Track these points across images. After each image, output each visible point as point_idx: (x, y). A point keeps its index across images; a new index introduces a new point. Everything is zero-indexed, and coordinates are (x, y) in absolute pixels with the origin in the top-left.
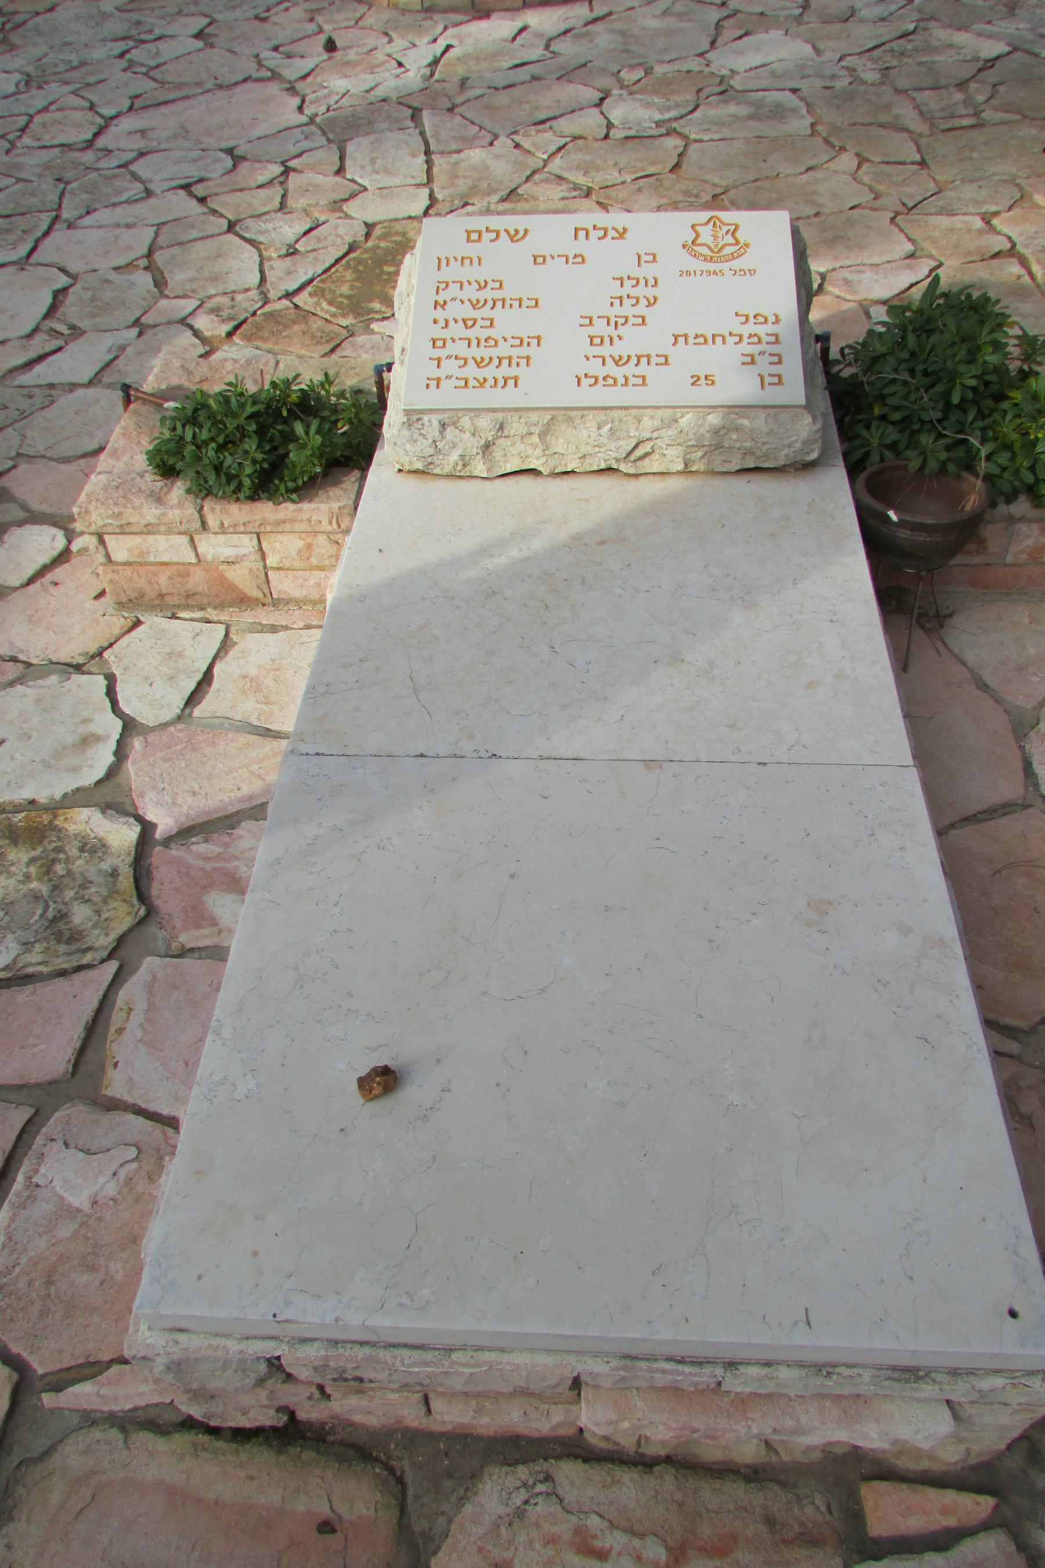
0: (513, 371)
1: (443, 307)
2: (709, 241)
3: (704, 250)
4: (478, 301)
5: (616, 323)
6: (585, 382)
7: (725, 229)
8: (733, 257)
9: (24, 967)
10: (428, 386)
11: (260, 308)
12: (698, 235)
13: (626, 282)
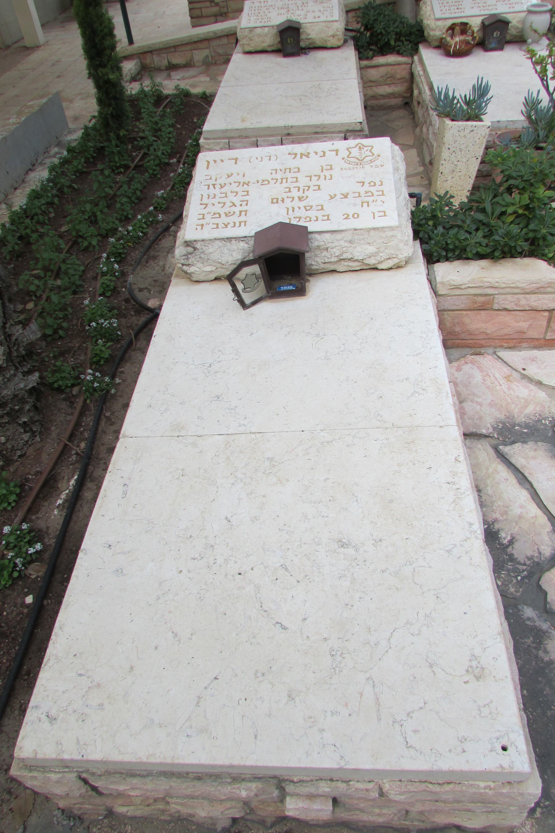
4: (230, 213)
5: (304, 189)
12: (350, 153)
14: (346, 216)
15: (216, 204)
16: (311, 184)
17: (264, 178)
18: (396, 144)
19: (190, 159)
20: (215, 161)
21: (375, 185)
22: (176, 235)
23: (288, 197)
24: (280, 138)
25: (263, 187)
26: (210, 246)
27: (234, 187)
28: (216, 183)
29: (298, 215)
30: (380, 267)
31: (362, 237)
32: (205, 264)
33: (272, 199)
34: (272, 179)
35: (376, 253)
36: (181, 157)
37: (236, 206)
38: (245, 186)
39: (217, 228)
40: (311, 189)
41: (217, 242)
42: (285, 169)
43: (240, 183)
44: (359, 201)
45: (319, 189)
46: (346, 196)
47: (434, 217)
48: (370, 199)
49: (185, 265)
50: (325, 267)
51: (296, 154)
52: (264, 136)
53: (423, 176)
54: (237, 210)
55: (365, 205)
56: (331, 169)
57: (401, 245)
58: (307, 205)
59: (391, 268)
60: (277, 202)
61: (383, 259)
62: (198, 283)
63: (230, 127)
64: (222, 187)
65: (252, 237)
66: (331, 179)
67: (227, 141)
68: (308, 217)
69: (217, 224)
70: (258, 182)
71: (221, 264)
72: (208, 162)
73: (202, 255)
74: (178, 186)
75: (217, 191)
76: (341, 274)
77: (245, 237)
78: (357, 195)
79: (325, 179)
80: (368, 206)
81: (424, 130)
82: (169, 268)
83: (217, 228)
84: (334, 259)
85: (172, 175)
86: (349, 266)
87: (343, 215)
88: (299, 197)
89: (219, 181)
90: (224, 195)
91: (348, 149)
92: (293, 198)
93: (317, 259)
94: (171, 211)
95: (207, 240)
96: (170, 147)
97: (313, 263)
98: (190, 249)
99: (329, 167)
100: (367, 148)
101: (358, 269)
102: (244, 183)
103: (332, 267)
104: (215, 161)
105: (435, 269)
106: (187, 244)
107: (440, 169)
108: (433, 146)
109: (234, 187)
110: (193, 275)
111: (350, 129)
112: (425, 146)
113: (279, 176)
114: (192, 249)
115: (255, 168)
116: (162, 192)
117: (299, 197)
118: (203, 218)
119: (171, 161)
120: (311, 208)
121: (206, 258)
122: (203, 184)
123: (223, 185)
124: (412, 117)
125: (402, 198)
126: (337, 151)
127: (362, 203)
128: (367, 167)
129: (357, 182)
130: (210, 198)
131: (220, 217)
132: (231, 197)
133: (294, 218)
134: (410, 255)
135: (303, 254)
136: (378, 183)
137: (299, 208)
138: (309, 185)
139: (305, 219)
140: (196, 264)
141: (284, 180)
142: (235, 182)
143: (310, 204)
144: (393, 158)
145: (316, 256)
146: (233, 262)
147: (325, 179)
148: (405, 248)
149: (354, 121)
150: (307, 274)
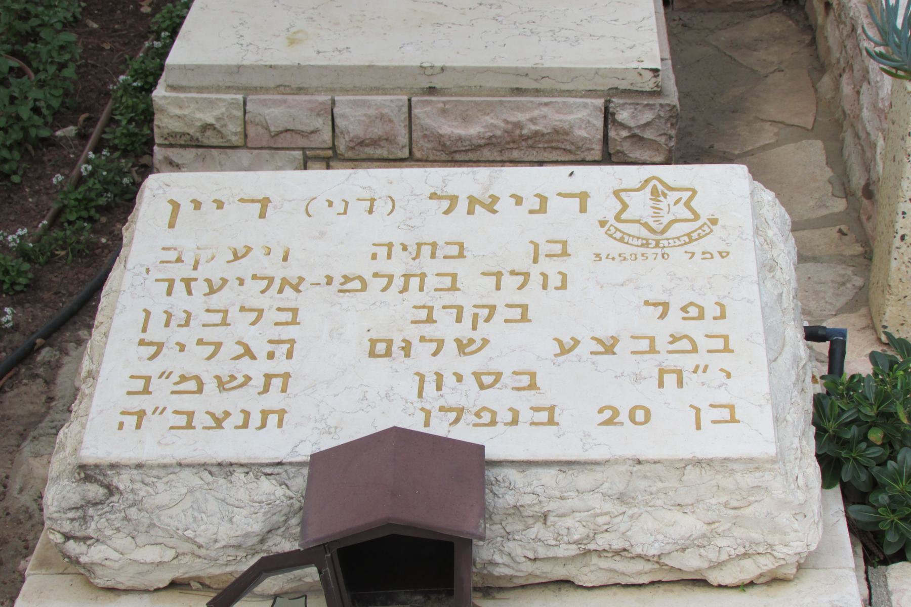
4: (233, 378)
5: (475, 317)
10: (121, 426)
12: (625, 206)
13: (507, 280)
14: (608, 414)
15: (191, 345)
16: (498, 299)
17: (351, 271)
18: (768, 185)
19: (119, 131)
20: (197, 205)
21: (701, 317)
22: (55, 376)
23: (423, 339)
24: (406, 98)
25: (346, 298)
26: (160, 486)
27: (252, 293)
28: (194, 274)
29: (452, 399)
30: (714, 577)
31: (660, 485)
32: (141, 539)
33: (373, 342)
34: (376, 275)
35: (704, 536)
36: (91, 122)
37: (253, 357)
38: (288, 290)
39: (190, 426)
40: (497, 318)
41: (186, 474)
42: (419, 245)
43: (271, 280)
44: (649, 366)
45: (524, 318)
46: (609, 347)
47: (887, 418)
48: (686, 362)
49: (76, 539)
50: (538, 572)
51: (454, 199)
52: (355, 90)
53: (844, 228)
54: (257, 369)
55: (670, 380)
56: (565, 253)
57: (784, 518)
58: (482, 369)
59: (752, 584)
60: (388, 353)
61: (724, 557)
62: (111, 595)
63: (250, 59)
64: (212, 291)
65: (301, 464)
66: (563, 286)
67: (240, 97)
68: (484, 409)
69: (190, 415)
70: (330, 280)
71: (195, 543)
72: (176, 206)
73: (133, 512)
74: (72, 217)
75: (197, 303)
76: (586, 593)
77: (280, 464)
78: (644, 345)
79: (545, 287)
80: (680, 384)
81: (847, 89)
82: (21, 490)
83: (190, 426)
84: (563, 551)
85: (58, 178)
86: (615, 571)
87: (601, 411)
88: (458, 341)
89: (204, 272)
90: (217, 318)
91: (617, 193)
92: (441, 343)
93: (510, 546)
94: (46, 296)
95: (151, 467)
96: (61, 92)
97: (498, 558)
98: (94, 491)
99: (558, 248)
100: (677, 195)
101: (645, 580)
102: (285, 281)
103: (560, 572)
104: (197, 205)
105: (892, 583)
106: (87, 473)
107: (898, 226)
108: (874, 146)
109: (252, 293)
110: (99, 571)
111: (623, 85)
112: (848, 136)
113: (398, 266)
114: (102, 491)
115: (322, 234)
116: (20, 232)
117: (458, 341)
118: (146, 391)
119: (59, 133)
120: (496, 381)
121: (146, 521)
122: (155, 274)
123: (217, 283)
124: (807, 38)
125: (786, 359)
126: (583, 197)
127: (662, 372)
128: (677, 254)
129: (647, 303)
130: (173, 323)
131: (200, 390)
132: (240, 327)
133: (442, 409)
134: (813, 548)
135: (468, 543)
136: (712, 311)
137: (459, 378)
138: (491, 302)
139: (478, 415)
140: (110, 538)
141: (415, 282)
142: (254, 277)
143: (494, 367)
144: (757, 230)
145: (508, 536)
146: (233, 542)
147: (545, 287)
148: (796, 525)
149: (635, 65)
150: (476, 589)
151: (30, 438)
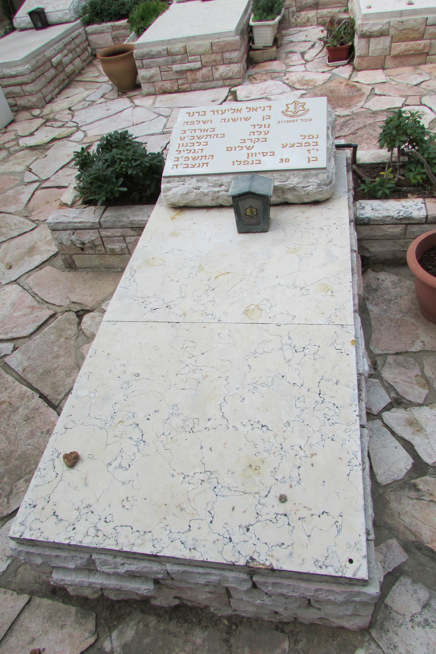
0: (206, 161)
1: (240, 111)
2: (293, 110)
3: (291, 113)
6: (236, 163)
7: (300, 105)
8: (302, 115)
9: (136, 138)
11: (333, 603)
12: (288, 108)
21: (313, 138)
69: (188, 165)
79: (265, 127)
91: (287, 105)
151: (278, 617)
